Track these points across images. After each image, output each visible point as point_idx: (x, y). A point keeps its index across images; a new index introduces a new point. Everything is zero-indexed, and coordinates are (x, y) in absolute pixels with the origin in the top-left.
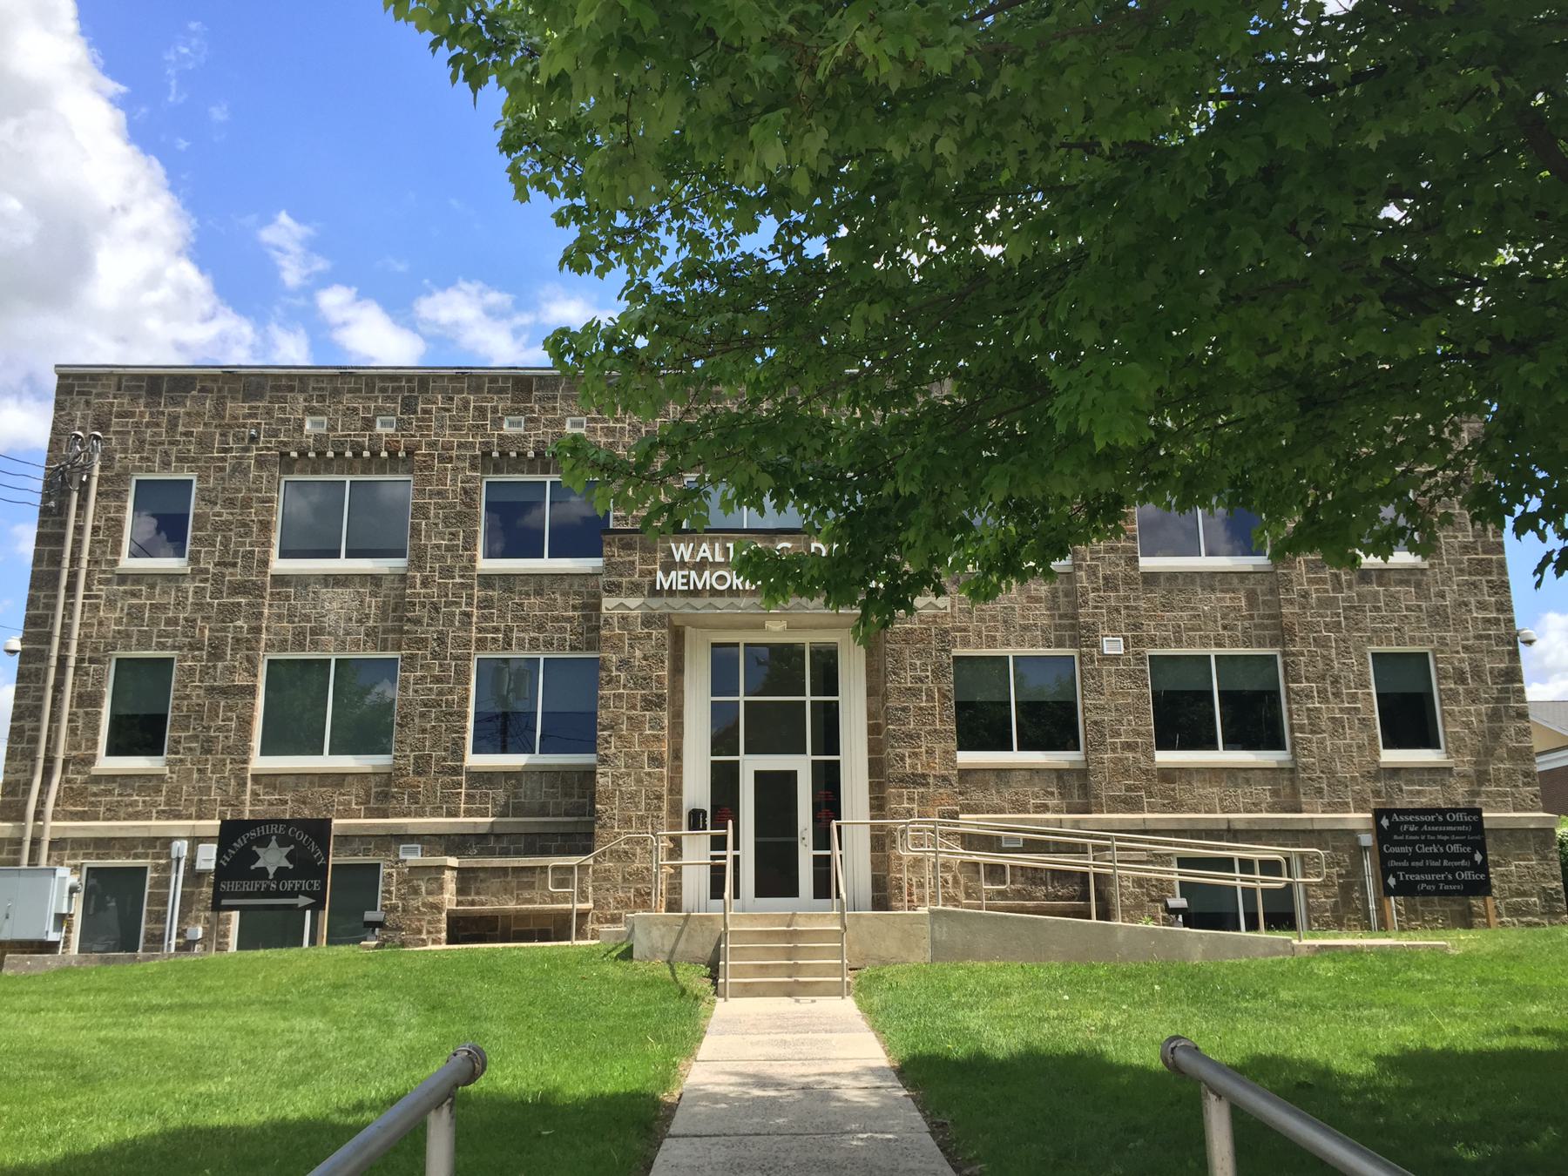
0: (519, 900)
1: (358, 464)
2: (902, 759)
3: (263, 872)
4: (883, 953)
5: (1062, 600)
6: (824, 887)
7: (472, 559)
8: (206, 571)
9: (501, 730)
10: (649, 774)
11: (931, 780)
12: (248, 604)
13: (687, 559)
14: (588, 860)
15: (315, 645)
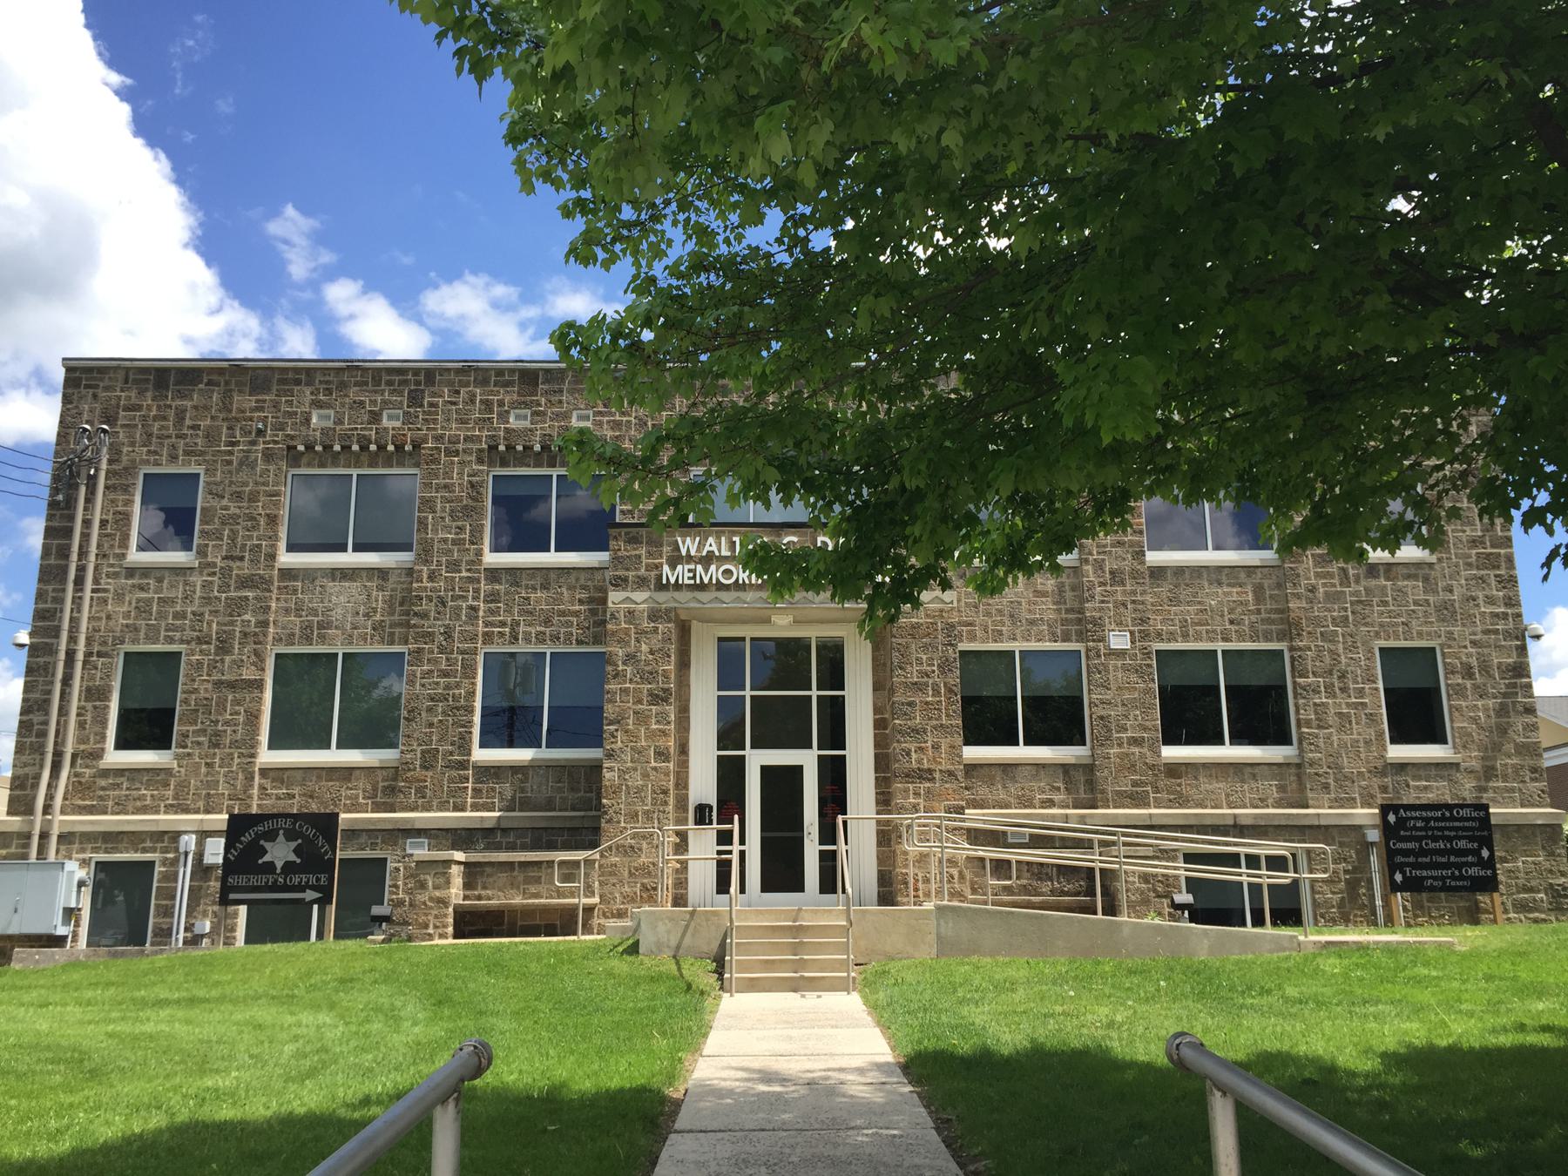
0: (525, 894)
1: (364, 458)
2: (908, 754)
3: (270, 867)
5: (1069, 594)
6: (830, 882)
7: (479, 553)
8: (214, 565)
9: (508, 724)
10: (655, 769)
11: (937, 775)
12: (255, 598)
13: (693, 553)
14: (594, 854)
15: (323, 639)
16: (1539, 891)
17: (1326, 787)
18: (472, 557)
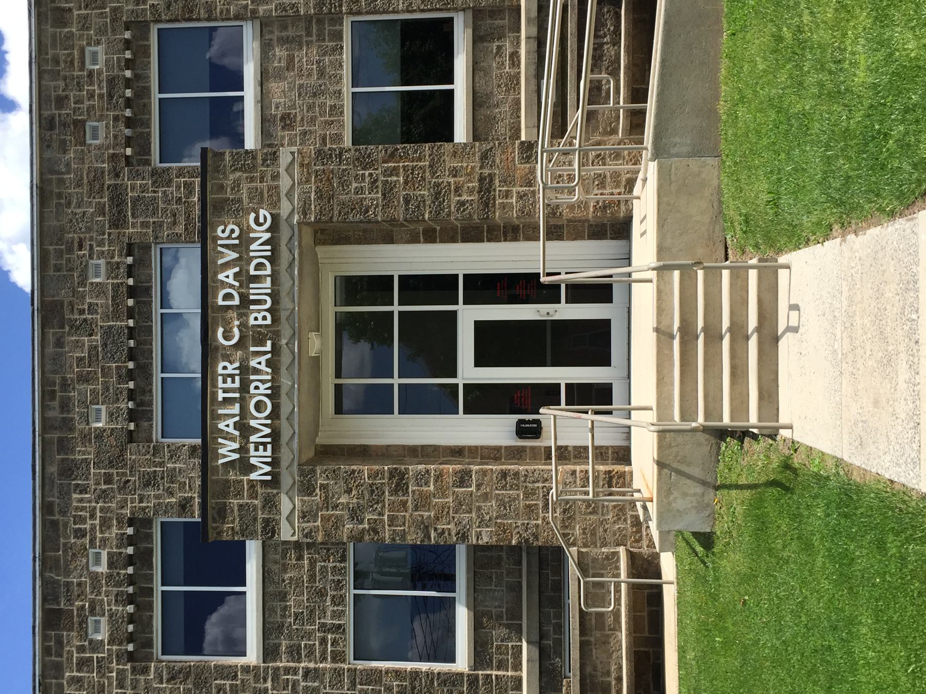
2: (462, 204)
4: (706, 219)
5: (290, 32)
6: (600, 292)
7: (246, 669)
10: (479, 486)
11: (486, 171)
13: (236, 446)
14: (572, 553)
18: (250, 677)
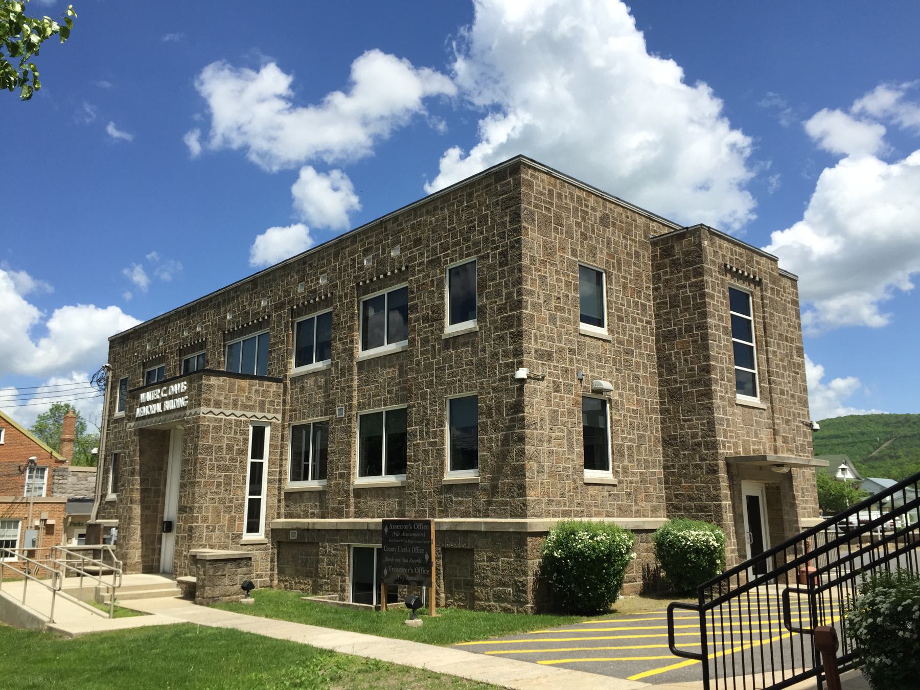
16: (508, 586)
17: (414, 502)
